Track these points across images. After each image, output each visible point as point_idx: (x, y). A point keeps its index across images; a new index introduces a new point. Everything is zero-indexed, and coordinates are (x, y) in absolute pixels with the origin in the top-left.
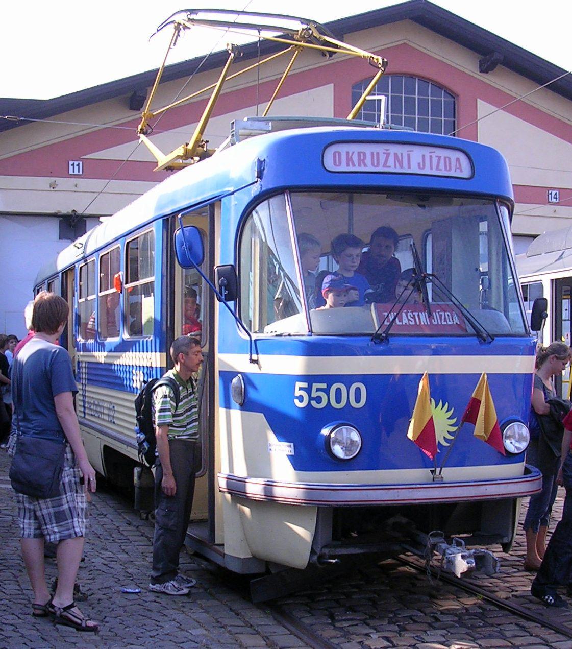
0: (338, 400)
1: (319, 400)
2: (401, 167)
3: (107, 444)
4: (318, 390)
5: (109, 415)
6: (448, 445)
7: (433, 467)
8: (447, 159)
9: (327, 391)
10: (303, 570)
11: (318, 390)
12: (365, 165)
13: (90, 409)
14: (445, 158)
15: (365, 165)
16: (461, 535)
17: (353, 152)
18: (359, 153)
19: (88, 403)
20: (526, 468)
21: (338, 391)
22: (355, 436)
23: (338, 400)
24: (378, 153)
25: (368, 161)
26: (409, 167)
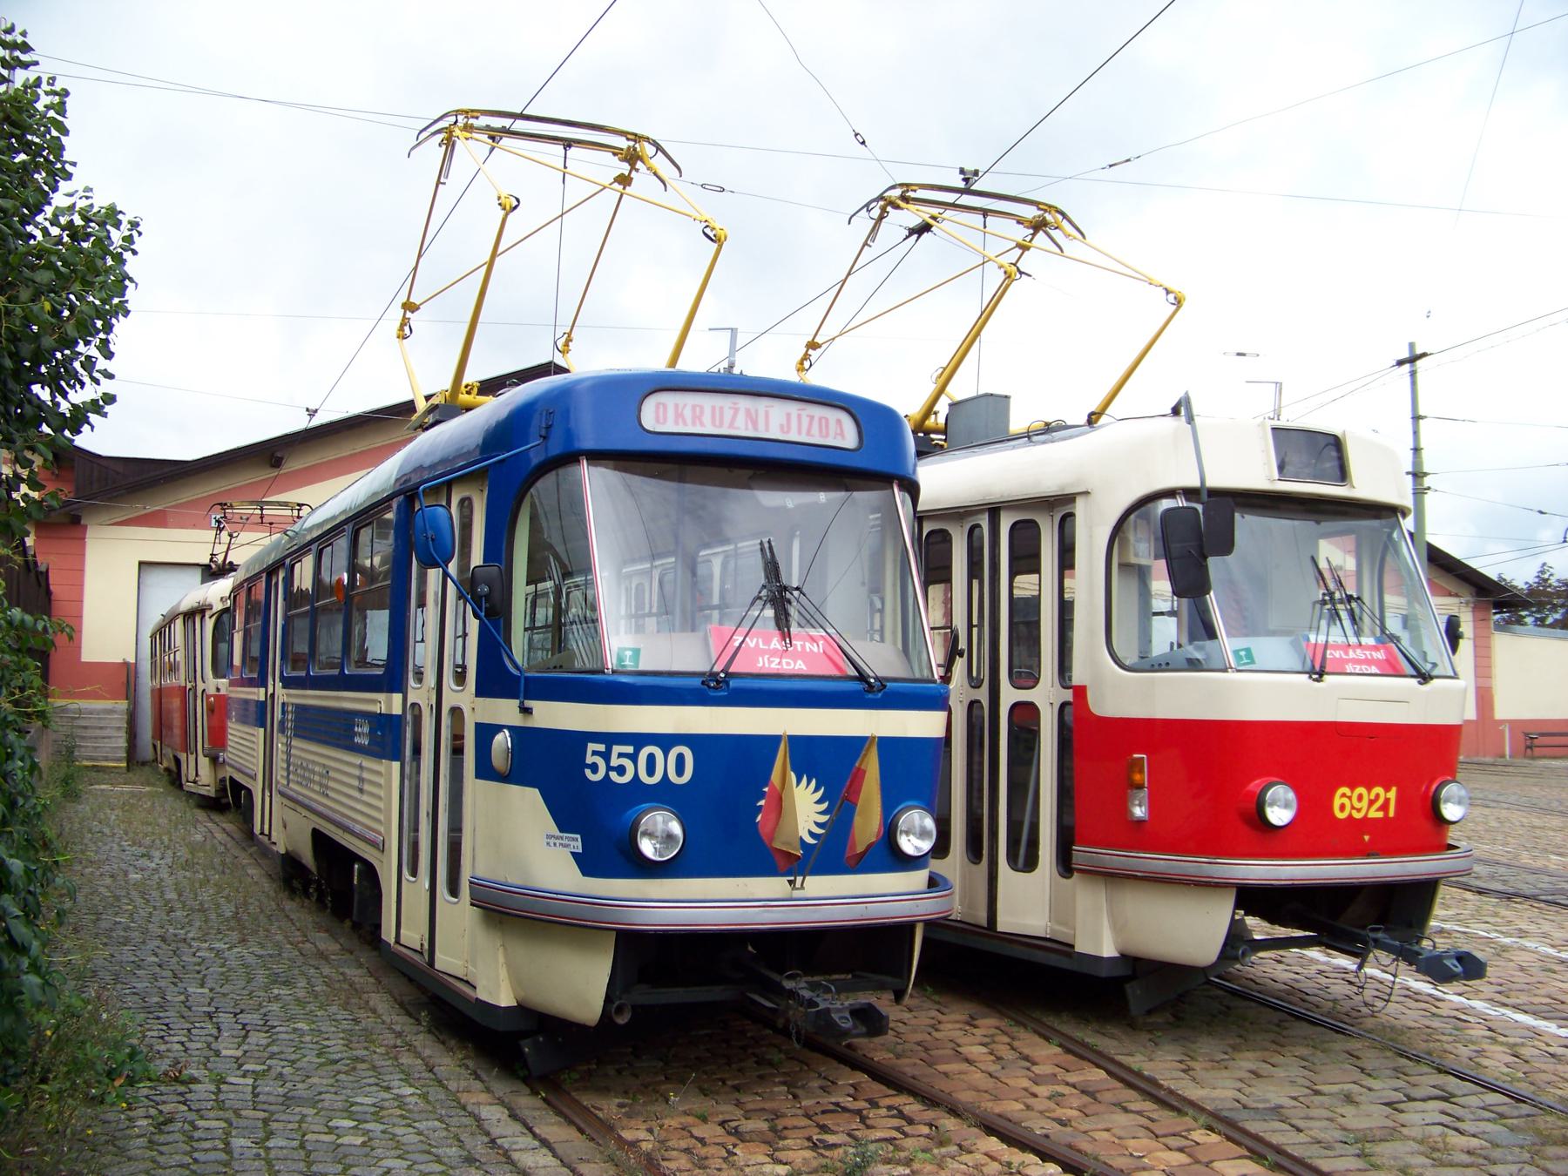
0: (651, 771)
1: (621, 770)
2: (755, 427)
3: (317, 827)
4: (621, 755)
5: (321, 785)
6: (815, 842)
7: (791, 875)
8: (823, 421)
9: (634, 758)
10: (590, 1027)
11: (621, 755)
12: (702, 424)
13: (295, 773)
14: (820, 419)
15: (702, 424)
16: (835, 977)
17: (685, 405)
18: (694, 407)
19: (294, 765)
20: (38, 1010)
21: (651, 759)
22: (676, 828)
23: (650, 772)
24: (721, 408)
25: (707, 418)
26: (767, 429)
